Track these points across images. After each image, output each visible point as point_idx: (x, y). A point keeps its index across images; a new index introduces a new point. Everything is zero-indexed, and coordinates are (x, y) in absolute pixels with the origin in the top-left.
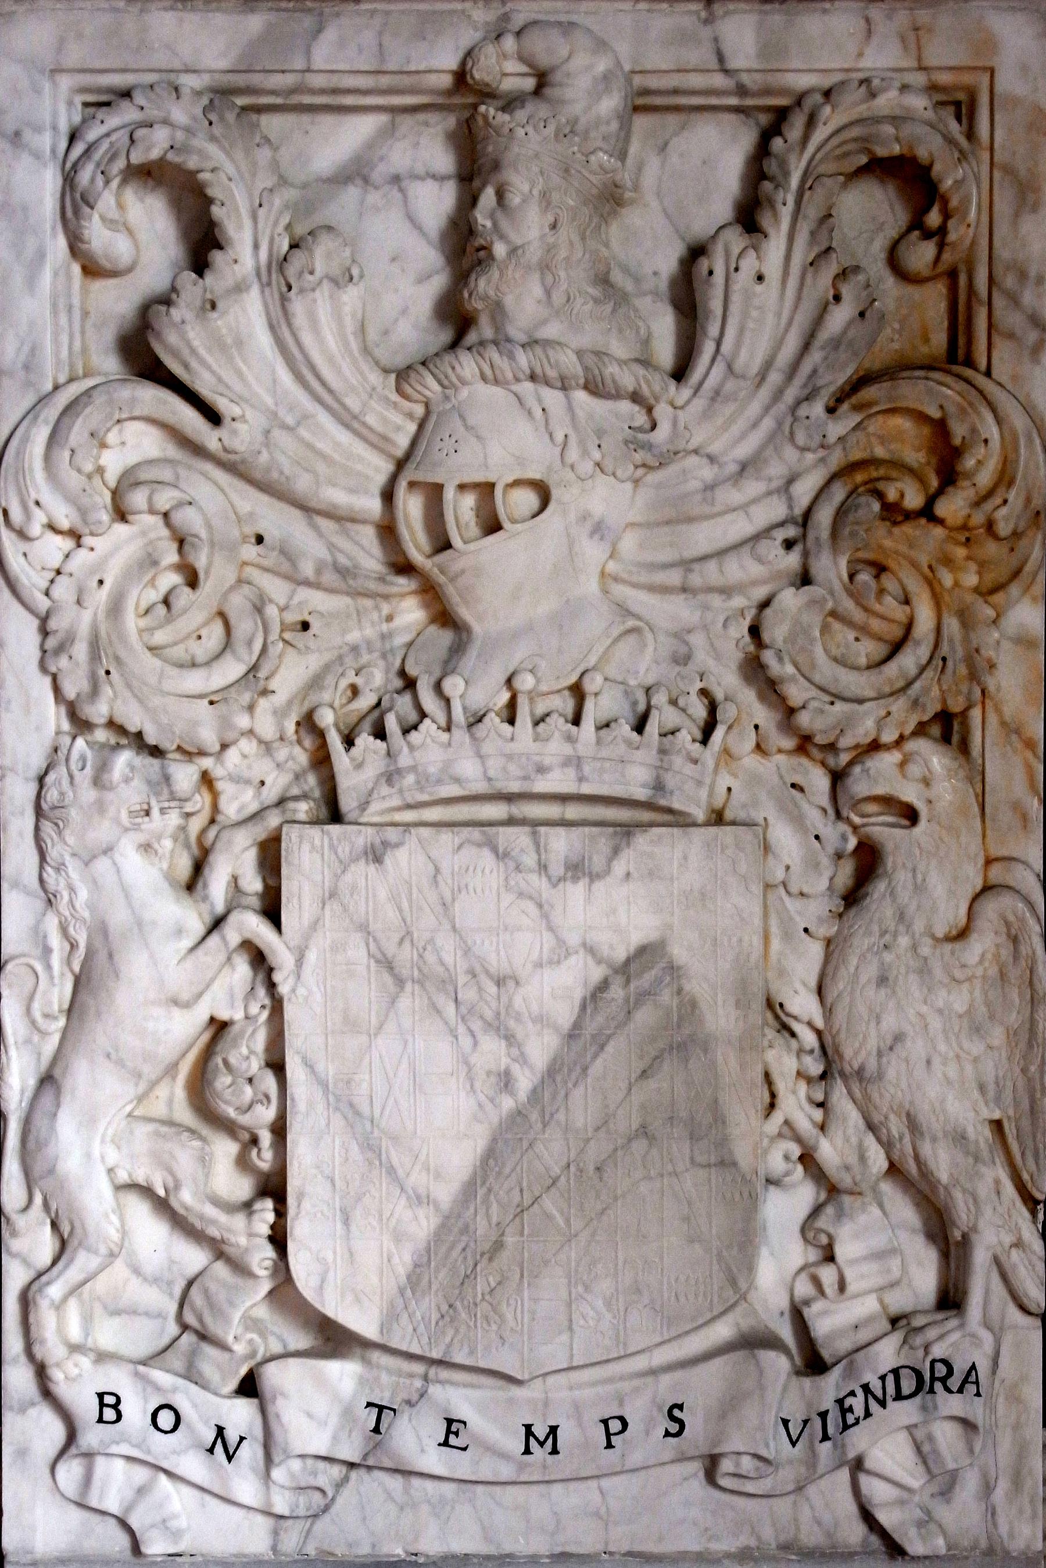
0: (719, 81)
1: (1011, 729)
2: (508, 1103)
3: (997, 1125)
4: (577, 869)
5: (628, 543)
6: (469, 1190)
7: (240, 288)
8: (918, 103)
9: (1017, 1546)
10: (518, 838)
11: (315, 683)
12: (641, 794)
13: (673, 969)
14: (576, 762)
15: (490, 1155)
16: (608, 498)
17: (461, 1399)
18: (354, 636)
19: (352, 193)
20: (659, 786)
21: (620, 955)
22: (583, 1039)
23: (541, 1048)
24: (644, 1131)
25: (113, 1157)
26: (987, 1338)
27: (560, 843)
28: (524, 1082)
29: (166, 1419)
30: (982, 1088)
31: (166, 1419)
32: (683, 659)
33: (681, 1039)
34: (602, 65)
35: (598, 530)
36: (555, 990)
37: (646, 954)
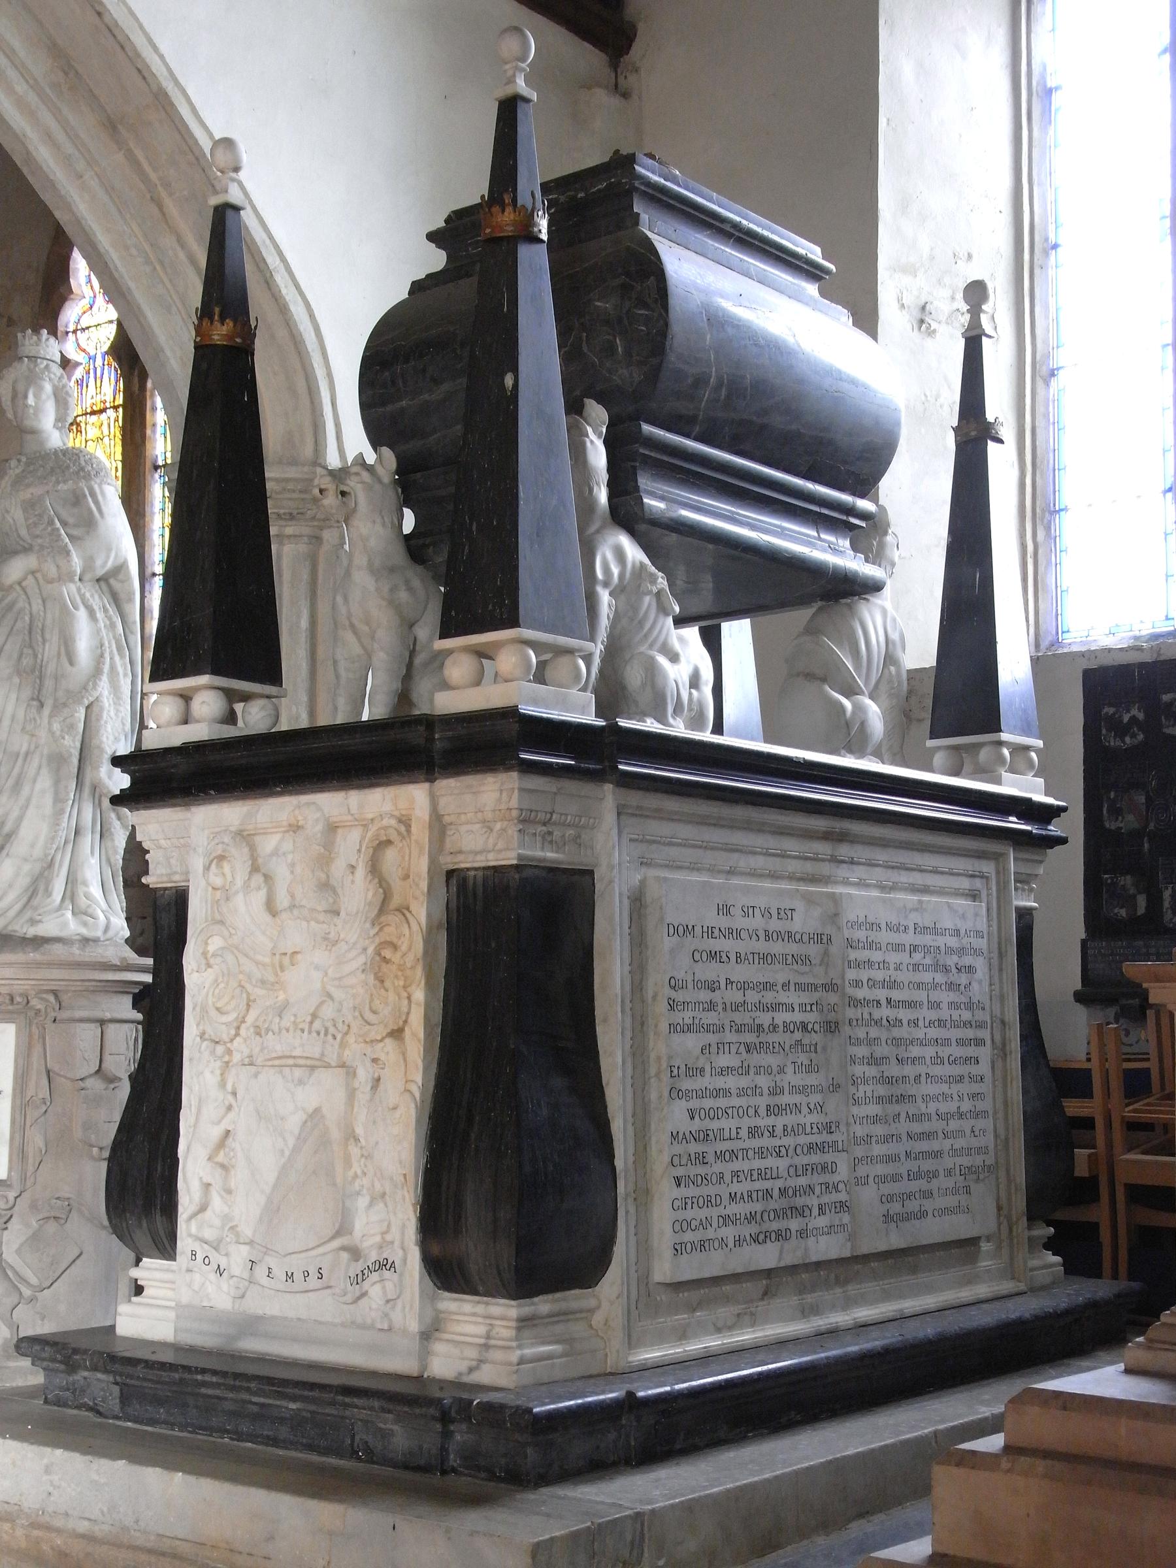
0: (350, 818)
1: (414, 1035)
2: (283, 1160)
3: (405, 1175)
4: (301, 1082)
5: (330, 971)
6: (275, 1187)
7: (237, 892)
8: (393, 822)
9: (411, 1329)
10: (287, 1071)
11: (257, 1020)
12: (317, 1056)
13: (323, 1117)
14: (302, 1045)
15: (278, 1178)
16: (320, 956)
17: (271, 1261)
18: (268, 1004)
19: (274, 858)
20: (323, 1055)
21: (311, 1111)
22: (301, 1139)
23: (291, 1142)
24: (314, 1172)
25: (202, 1174)
26: (401, 1253)
27: (298, 1073)
28: (287, 1153)
29: (207, 1261)
30: (401, 1162)
31: (207, 1261)
32: (339, 1011)
33: (324, 1142)
34: (318, 815)
35: (317, 968)
36: (294, 1122)
37: (317, 1110)
